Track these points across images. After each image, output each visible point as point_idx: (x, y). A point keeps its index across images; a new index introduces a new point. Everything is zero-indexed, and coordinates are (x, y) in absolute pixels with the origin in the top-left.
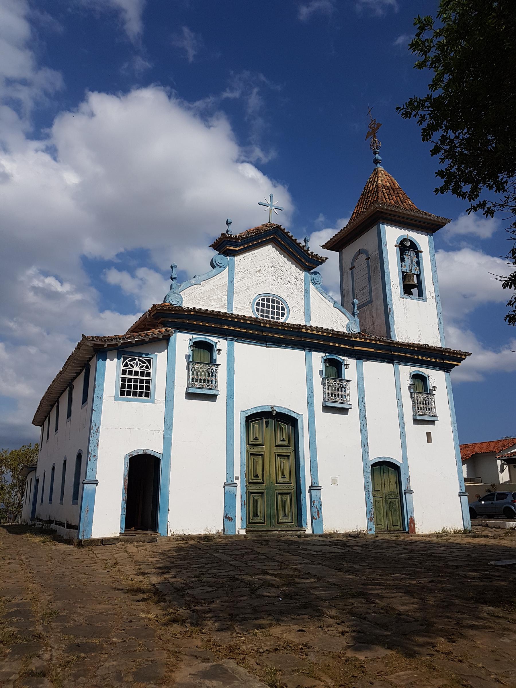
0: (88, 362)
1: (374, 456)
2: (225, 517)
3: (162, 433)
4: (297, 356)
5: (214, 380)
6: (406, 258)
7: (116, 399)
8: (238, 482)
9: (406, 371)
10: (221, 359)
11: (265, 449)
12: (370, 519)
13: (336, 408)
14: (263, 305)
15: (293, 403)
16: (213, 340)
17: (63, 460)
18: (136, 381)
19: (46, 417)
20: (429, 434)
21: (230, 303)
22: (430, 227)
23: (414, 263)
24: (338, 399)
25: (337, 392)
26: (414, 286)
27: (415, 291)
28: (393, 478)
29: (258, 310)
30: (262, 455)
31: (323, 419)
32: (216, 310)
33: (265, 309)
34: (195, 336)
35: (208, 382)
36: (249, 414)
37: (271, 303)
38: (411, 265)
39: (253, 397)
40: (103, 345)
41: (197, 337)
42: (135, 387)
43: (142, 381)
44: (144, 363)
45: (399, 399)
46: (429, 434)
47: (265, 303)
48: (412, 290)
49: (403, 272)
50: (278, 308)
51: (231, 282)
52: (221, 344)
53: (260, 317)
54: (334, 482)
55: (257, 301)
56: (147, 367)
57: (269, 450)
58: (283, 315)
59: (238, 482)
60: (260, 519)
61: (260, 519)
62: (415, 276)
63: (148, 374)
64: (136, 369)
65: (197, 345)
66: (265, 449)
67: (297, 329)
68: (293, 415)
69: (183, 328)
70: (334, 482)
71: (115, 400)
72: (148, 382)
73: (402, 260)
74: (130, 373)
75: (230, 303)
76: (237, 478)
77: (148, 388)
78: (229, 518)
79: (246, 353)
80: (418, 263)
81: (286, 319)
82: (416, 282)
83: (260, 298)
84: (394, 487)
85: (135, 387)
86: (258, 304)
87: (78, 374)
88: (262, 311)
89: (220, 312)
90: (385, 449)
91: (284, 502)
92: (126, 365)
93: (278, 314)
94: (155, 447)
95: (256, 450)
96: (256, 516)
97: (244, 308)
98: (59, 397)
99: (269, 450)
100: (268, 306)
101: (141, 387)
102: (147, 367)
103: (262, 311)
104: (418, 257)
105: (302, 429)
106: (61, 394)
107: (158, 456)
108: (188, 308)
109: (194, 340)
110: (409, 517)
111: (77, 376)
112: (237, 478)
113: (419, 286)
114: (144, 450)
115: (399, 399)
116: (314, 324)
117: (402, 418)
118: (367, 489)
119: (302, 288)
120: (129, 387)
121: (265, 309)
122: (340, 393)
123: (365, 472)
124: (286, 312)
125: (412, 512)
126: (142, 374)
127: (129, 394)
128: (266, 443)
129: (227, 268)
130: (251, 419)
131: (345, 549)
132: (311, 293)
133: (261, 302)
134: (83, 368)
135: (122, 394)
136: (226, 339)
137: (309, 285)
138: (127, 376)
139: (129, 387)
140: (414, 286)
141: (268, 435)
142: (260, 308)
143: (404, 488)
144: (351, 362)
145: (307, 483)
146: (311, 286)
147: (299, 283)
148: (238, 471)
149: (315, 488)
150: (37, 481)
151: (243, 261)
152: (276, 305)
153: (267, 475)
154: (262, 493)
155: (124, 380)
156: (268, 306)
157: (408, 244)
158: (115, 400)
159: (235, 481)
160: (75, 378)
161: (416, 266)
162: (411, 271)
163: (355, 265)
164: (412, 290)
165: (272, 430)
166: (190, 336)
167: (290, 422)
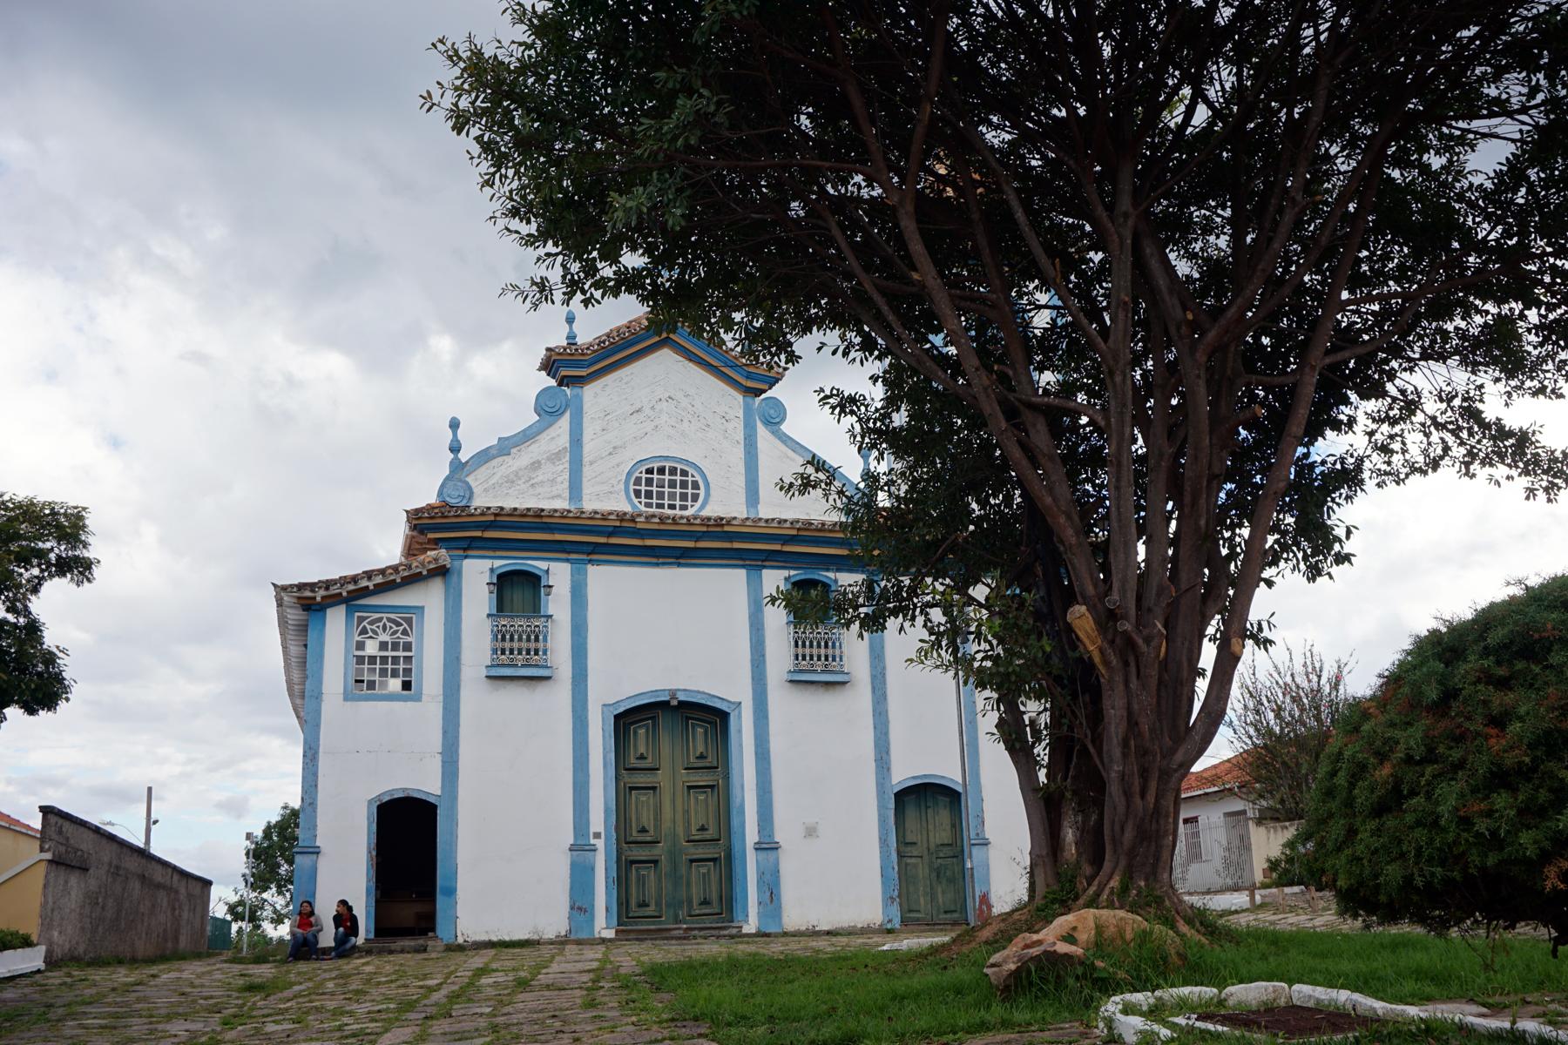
1: (904, 773)
2: (572, 908)
3: (439, 758)
4: (734, 579)
5: (837, 652)
8: (600, 844)
10: (558, 604)
11: (662, 778)
12: (888, 900)
14: (649, 482)
15: (722, 681)
16: (538, 565)
21: (753, 496)
24: (819, 666)
25: (815, 651)
29: (637, 493)
30: (654, 788)
36: (621, 710)
39: (624, 678)
41: (502, 564)
43: (395, 660)
50: (684, 485)
51: (576, 441)
52: (558, 574)
53: (643, 508)
54: (811, 832)
56: (405, 632)
57: (670, 777)
58: (695, 498)
60: (651, 910)
61: (651, 910)
63: (408, 647)
66: (662, 778)
67: (718, 528)
68: (719, 705)
69: (469, 546)
71: (346, 699)
75: (753, 496)
76: (597, 835)
78: (580, 907)
79: (615, 587)
81: (702, 507)
83: (644, 469)
86: (638, 481)
88: (649, 495)
91: (641, 881)
93: (684, 497)
94: (427, 784)
95: (641, 779)
96: (643, 904)
97: (607, 495)
99: (670, 777)
103: (649, 495)
105: (740, 731)
110: (978, 894)
112: (597, 835)
114: (404, 790)
116: (589, 505)
118: (883, 842)
119: (740, 436)
122: (532, 645)
123: (881, 807)
124: (702, 492)
125: (987, 881)
126: (395, 646)
128: (665, 763)
129: (567, 414)
130: (628, 721)
131: (833, 963)
133: (644, 476)
137: (754, 428)
141: (669, 752)
142: (643, 488)
145: (752, 835)
146: (759, 425)
147: (730, 426)
149: (768, 846)
153: (666, 825)
154: (655, 862)
158: (346, 699)
165: (673, 739)
166: (488, 564)
167: (709, 719)
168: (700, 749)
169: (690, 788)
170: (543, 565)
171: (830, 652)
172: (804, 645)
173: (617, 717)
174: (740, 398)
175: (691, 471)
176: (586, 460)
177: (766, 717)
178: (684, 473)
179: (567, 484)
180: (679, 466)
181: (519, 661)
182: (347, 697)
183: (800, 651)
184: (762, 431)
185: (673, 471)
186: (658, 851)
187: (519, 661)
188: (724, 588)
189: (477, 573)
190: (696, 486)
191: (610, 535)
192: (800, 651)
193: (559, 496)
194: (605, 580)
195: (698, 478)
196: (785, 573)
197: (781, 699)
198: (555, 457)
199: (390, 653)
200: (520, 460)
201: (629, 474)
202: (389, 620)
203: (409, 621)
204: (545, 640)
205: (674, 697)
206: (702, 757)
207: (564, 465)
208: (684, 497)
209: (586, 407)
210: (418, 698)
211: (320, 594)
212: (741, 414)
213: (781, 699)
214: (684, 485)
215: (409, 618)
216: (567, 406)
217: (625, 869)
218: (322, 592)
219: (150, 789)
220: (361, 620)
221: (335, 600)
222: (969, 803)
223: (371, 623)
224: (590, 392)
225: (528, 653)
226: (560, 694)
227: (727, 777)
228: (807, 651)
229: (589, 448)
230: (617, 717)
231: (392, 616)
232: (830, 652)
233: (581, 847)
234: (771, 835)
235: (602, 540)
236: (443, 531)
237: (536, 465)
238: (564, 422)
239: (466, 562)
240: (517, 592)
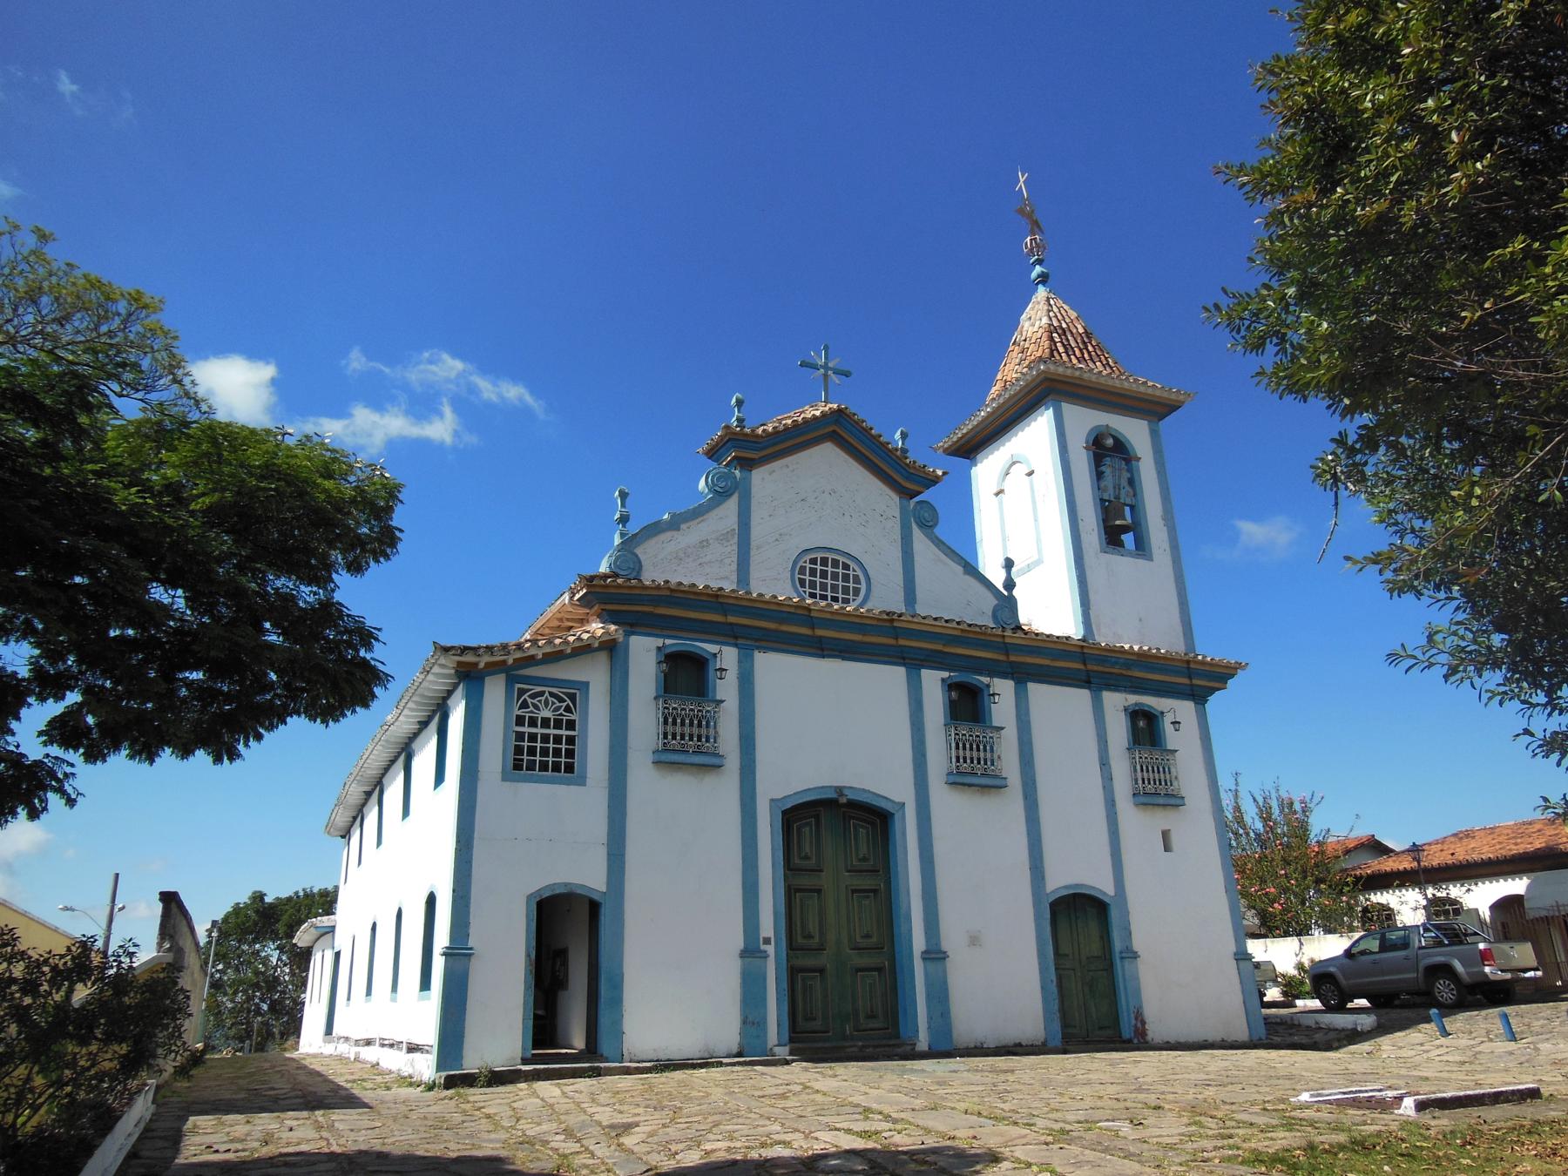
0: (445, 699)
1: (1060, 879)
6: (1107, 471)
7: (504, 779)
8: (770, 949)
9: (1116, 702)
10: (726, 689)
13: (975, 772)
14: (813, 572)
17: (1002, 561)
18: (545, 738)
19: (355, 818)
20: (1166, 835)
22: (1155, 410)
23: (1124, 483)
26: (1125, 529)
27: (1128, 539)
28: (1094, 927)
30: (819, 891)
31: (948, 805)
32: (715, 585)
33: (818, 580)
34: (668, 642)
35: (699, 739)
37: (826, 569)
38: (1117, 487)
39: (797, 762)
40: (476, 664)
42: (545, 752)
43: (558, 739)
44: (561, 700)
45: (1104, 763)
46: (1166, 835)
47: (819, 567)
48: (1123, 537)
49: (1102, 500)
50: (846, 578)
54: (974, 941)
55: (801, 563)
56: (568, 709)
59: (770, 949)
62: (1127, 509)
63: (571, 725)
64: (546, 713)
65: (950, 686)
67: (889, 623)
70: (974, 941)
72: (571, 740)
73: (1099, 475)
74: (533, 723)
77: (570, 753)
79: (777, 671)
80: (1131, 482)
82: (1129, 520)
84: (1095, 948)
85: (545, 752)
86: (803, 569)
87: (424, 724)
89: (721, 589)
90: (1078, 865)
92: (524, 705)
93: (846, 590)
94: (590, 876)
95: (805, 881)
97: (773, 582)
98: (383, 775)
100: (824, 574)
101: (557, 753)
102: (568, 709)
104: (1130, 470)
105: (904, 834)
106: (387, 769)
107: (596, 897)
108: (667, 582)
109: (668, 651)
111: (420, 731)
112: (767, 941)
113: (1137, 528)
114: (566, 885)
115: (1104, 763)
117: (1110, 803)
120: (532, 751)
121: (818, 580)
124: (863, 587)
127: (531, 767)
132: (919, 560)
134: (434, 712)
135: (517, 766)
136: (736, 645)
138: (526, 729)
139: (532, 751)
140: (1125, 529)
143: (1118, 945)
144: (1003, 688)
145: (919, 943)
146: (914, 526)
148: (767, 927)
149: (935, 955)
150: (338, 955)
151: (766, 481)
152: (840, 571)
155: (520, 736)
156: (824, 574)
157: (1110, 442)
158: (584, 784)
159: (763, 947)
160: (416, 735)
161: (1128, 488)
162: (1118, 498)
163: (1006, 486)
164: (1123, 537)
168: (863, 851)
169: (854, 891)
170: (712, 648)
171: (704, 731)
172: (674, 723)
173: (784, 813)
174: (896, 498)
175: (852, 565)
176: (753, 544)
177: (929, 819)
178: (846, 567)
179: (734, 566)
180: (841, 559)
181: (688, 745)
182: (505, 777)
183: (670, 729)
184: (917, 533)
185: (835, 563)
186: (822, 960)
187: (688, 745)
188: (884, 683)
189: (644, 652)
190: (857, 580)
191: (782, 621)
192: (670, 729)
193: (726, 578)
194: (772, 667)
195: (859, 573)
196: (946, 674)
197: (943, 799)
198: (723, 538)
199: (552, 731)
200: (691, 535)
201: (795, 563)
202: (551, 694)
203: (573, 697)
204: (992, 750)
205: (842, 795)
206: (864, 859)
207: (732, 548)
208: (846, 590)
209: (754, 490)
210: (582, 781)
211: (483, 661)
212: (897, 515)
213: (943, 799)
214: (846, 578)
215: (574, 695)
216: (736, 488)
217: (795, 976)
218: (487, 659)
219: (374, 925)
220: (522, 692)
221: (495, 668)
222: (1114, 914)
223: (533, 696)
224: (759, 476)
225: (699, 739)
226: (727, 785)
227: (888, 882)
228: (678, 729)
229: (757, 532)
230: (784, 813)
231: (554, 690)
232: (704, 731)
233: (751, 952)
234: (938, 944)
235: (772, 626)
236: (622, 600)
237: (704, 544)
238: (732, 504)
239: (634, 639)
240: (685, 676)
